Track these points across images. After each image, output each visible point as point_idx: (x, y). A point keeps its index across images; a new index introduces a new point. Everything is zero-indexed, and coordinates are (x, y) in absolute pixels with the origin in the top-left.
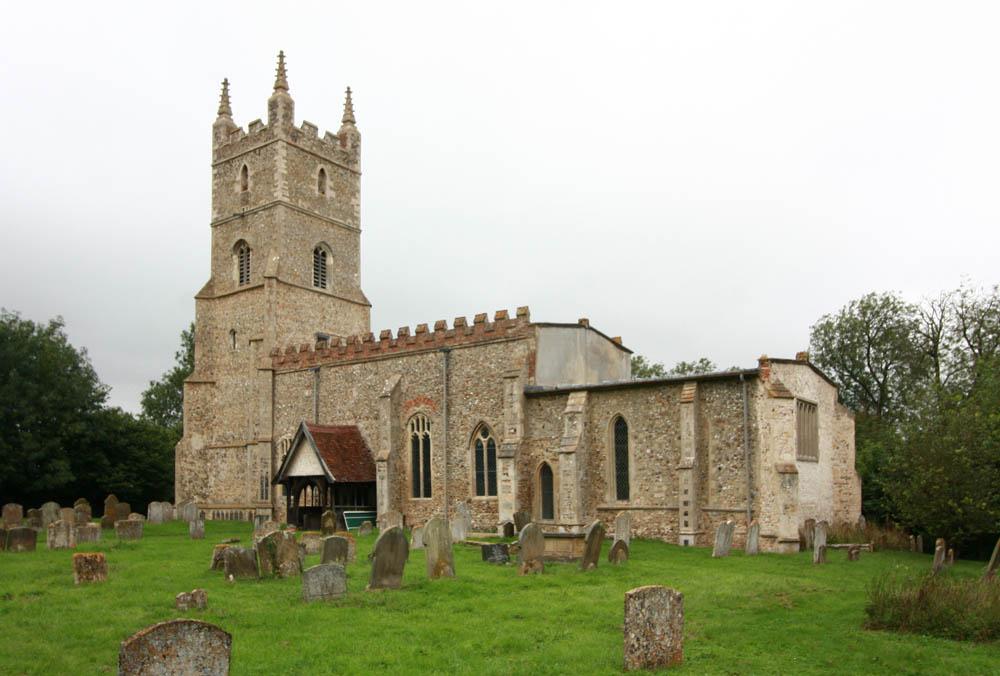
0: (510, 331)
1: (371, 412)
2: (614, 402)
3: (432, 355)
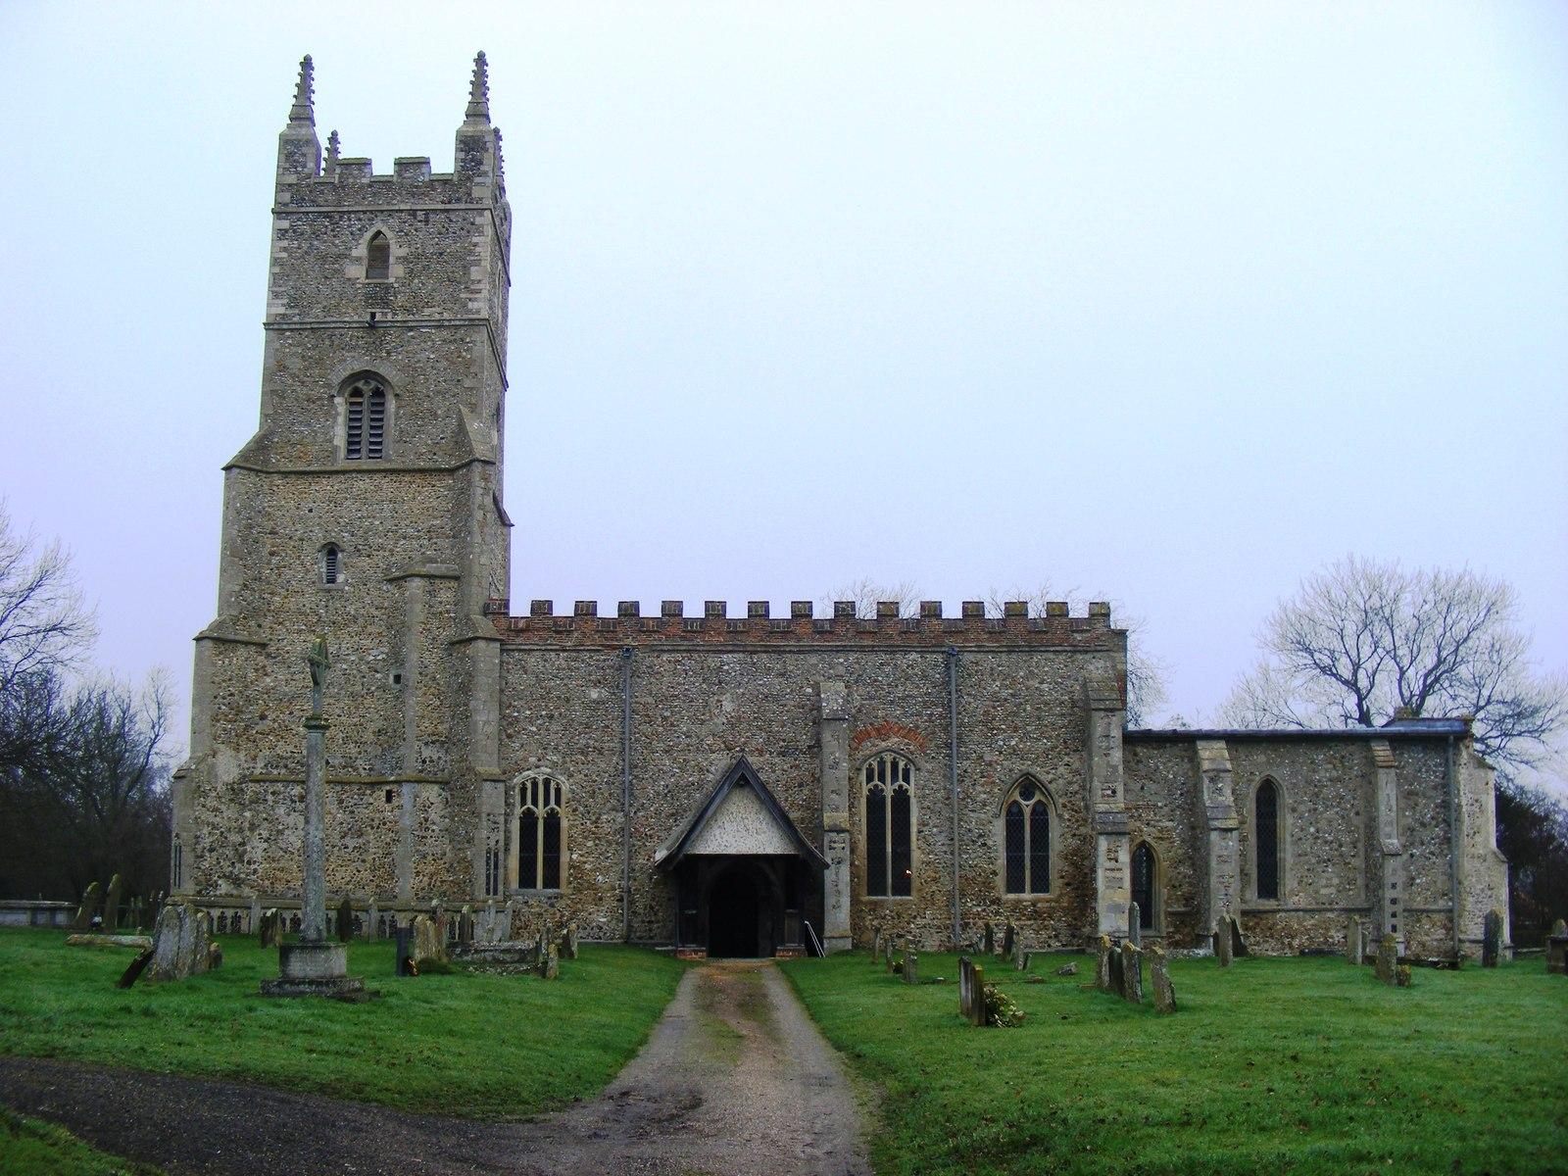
0: (1078, 637)
1: (768, 742)
2: (1262, 758)
3: (914, 656)
